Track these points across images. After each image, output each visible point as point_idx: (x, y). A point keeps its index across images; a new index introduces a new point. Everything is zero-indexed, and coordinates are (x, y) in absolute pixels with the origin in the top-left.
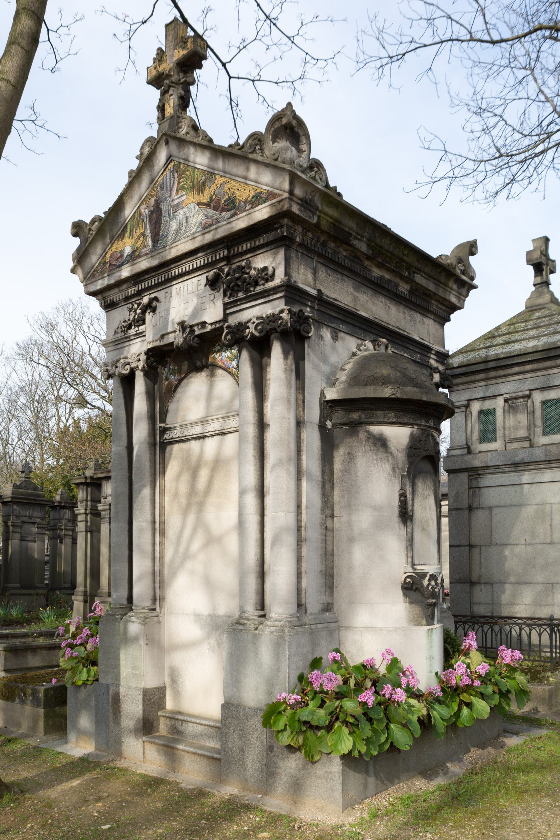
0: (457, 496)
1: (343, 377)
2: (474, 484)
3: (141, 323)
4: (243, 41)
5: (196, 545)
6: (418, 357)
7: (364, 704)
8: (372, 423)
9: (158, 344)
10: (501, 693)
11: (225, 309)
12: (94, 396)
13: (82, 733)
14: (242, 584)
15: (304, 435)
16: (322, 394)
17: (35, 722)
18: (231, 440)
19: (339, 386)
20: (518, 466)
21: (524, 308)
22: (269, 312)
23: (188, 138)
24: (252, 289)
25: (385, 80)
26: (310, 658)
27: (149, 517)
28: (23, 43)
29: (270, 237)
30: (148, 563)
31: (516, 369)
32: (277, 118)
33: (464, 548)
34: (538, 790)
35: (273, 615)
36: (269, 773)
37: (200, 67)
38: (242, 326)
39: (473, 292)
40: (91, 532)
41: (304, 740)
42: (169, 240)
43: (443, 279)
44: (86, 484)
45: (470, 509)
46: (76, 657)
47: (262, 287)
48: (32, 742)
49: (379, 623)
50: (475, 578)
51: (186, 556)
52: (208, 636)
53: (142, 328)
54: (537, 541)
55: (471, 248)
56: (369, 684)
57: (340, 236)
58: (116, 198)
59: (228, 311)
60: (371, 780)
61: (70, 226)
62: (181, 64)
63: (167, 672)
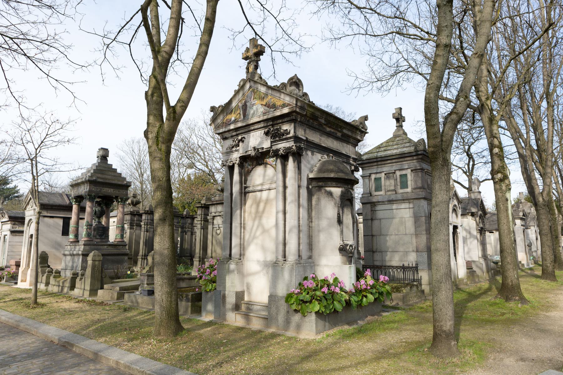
0: (366, 214)
1: (316, 169)
2: (373, 209)
4: (277, 38)
5: (258, 233)
6: (345, 160)
7: (324, 292)
8: (327, 187)
9: (244, 154)
10: (379, 293)
12: (199, 164)
13: (208, 312)
14: (277, 248)
15: (301, 191)
16: (308, 175)
17: (187, 309)
18: (273, 192)
19: (314, 173)
20: (391, 202)
21: (392, 136)
22: (288, 146)
23: (258, 81)
25: (333, 46)
26: (303, 277)
27: (239, 222)
28: (203, 55)
29: (288, 119)
30: (238, 240)
31: (389, 162)
32: (291, 79)
33: (370, 236)
34: (392, 329)
35: (289, 260)
36: (288, 322)
37: (262, 55)
38: (278, 150)
39: (366, 135)
40: (203, 229)
41: (301, 307)
42: (250, 116)
43: (354, 130)
44: (202, 207)
45: (372, 219)
46: (207, 280)
48: (186, 317)
49: (330, 264)
50: (374, 250)
51: (254, 237)
52: (263, 269)
53: (238, 148)
54: (399, 233)
55: (366, 118)
56: (326, 286)
57: (314, 117)
58: (229, 99)
60: (327, 324)
61: (209, 108)
62: (254, 55)
63: (245, 285)
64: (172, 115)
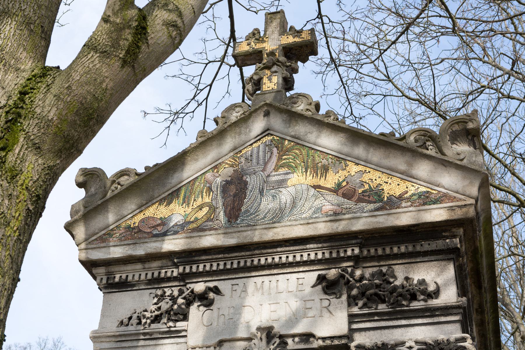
3: (181, 317)
11: (350, 323)
24: (404, 303)
47: (422, 303)
53: (180, 325)
59: (355, 326)
64: (128, 35)
